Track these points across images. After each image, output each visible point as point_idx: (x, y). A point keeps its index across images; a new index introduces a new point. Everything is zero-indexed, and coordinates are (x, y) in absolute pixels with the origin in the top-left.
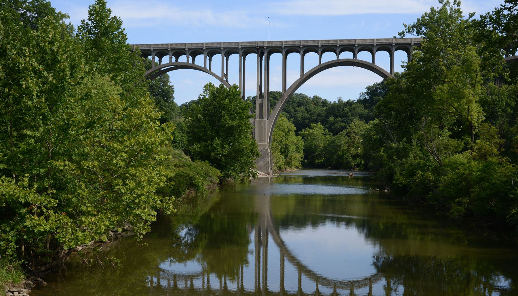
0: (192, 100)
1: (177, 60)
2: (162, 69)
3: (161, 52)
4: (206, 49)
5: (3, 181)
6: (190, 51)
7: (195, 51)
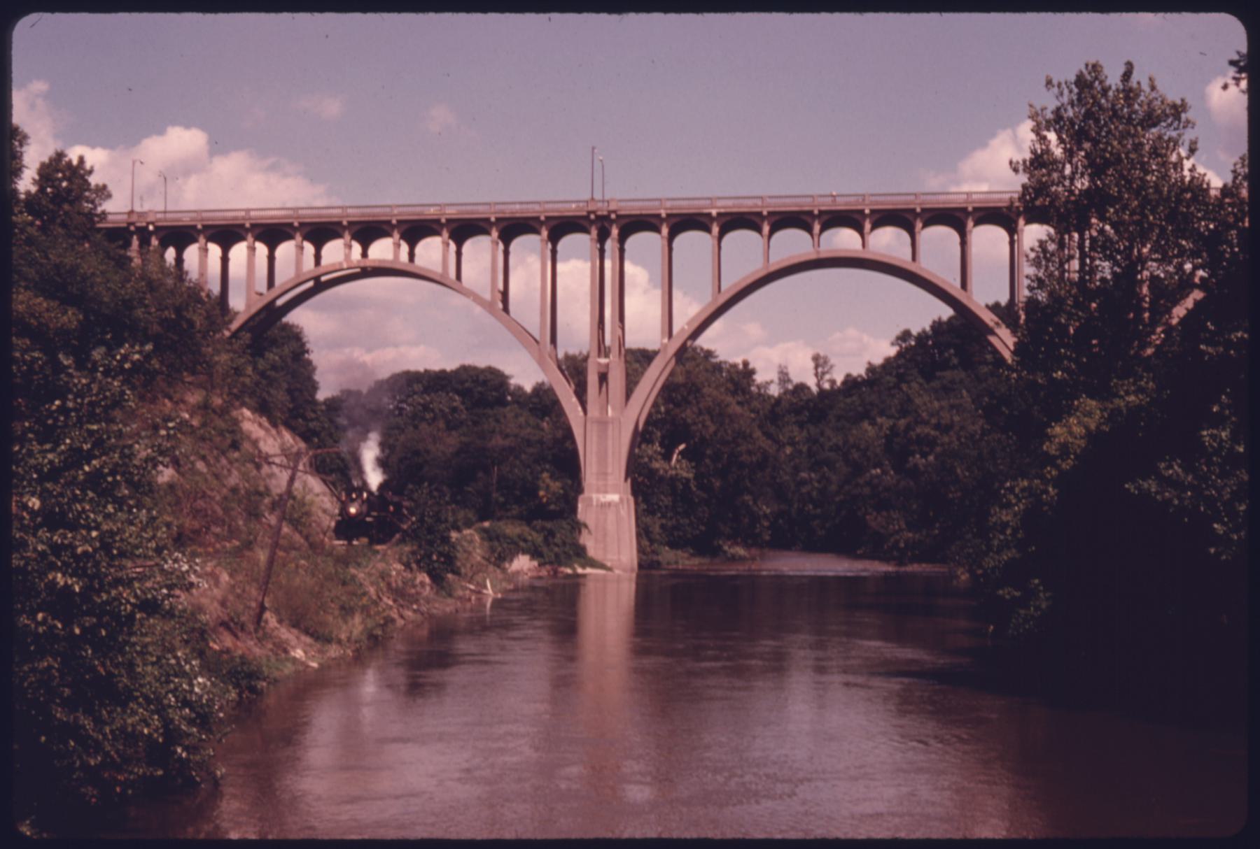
0: (318, 383)
7: (414, 231)
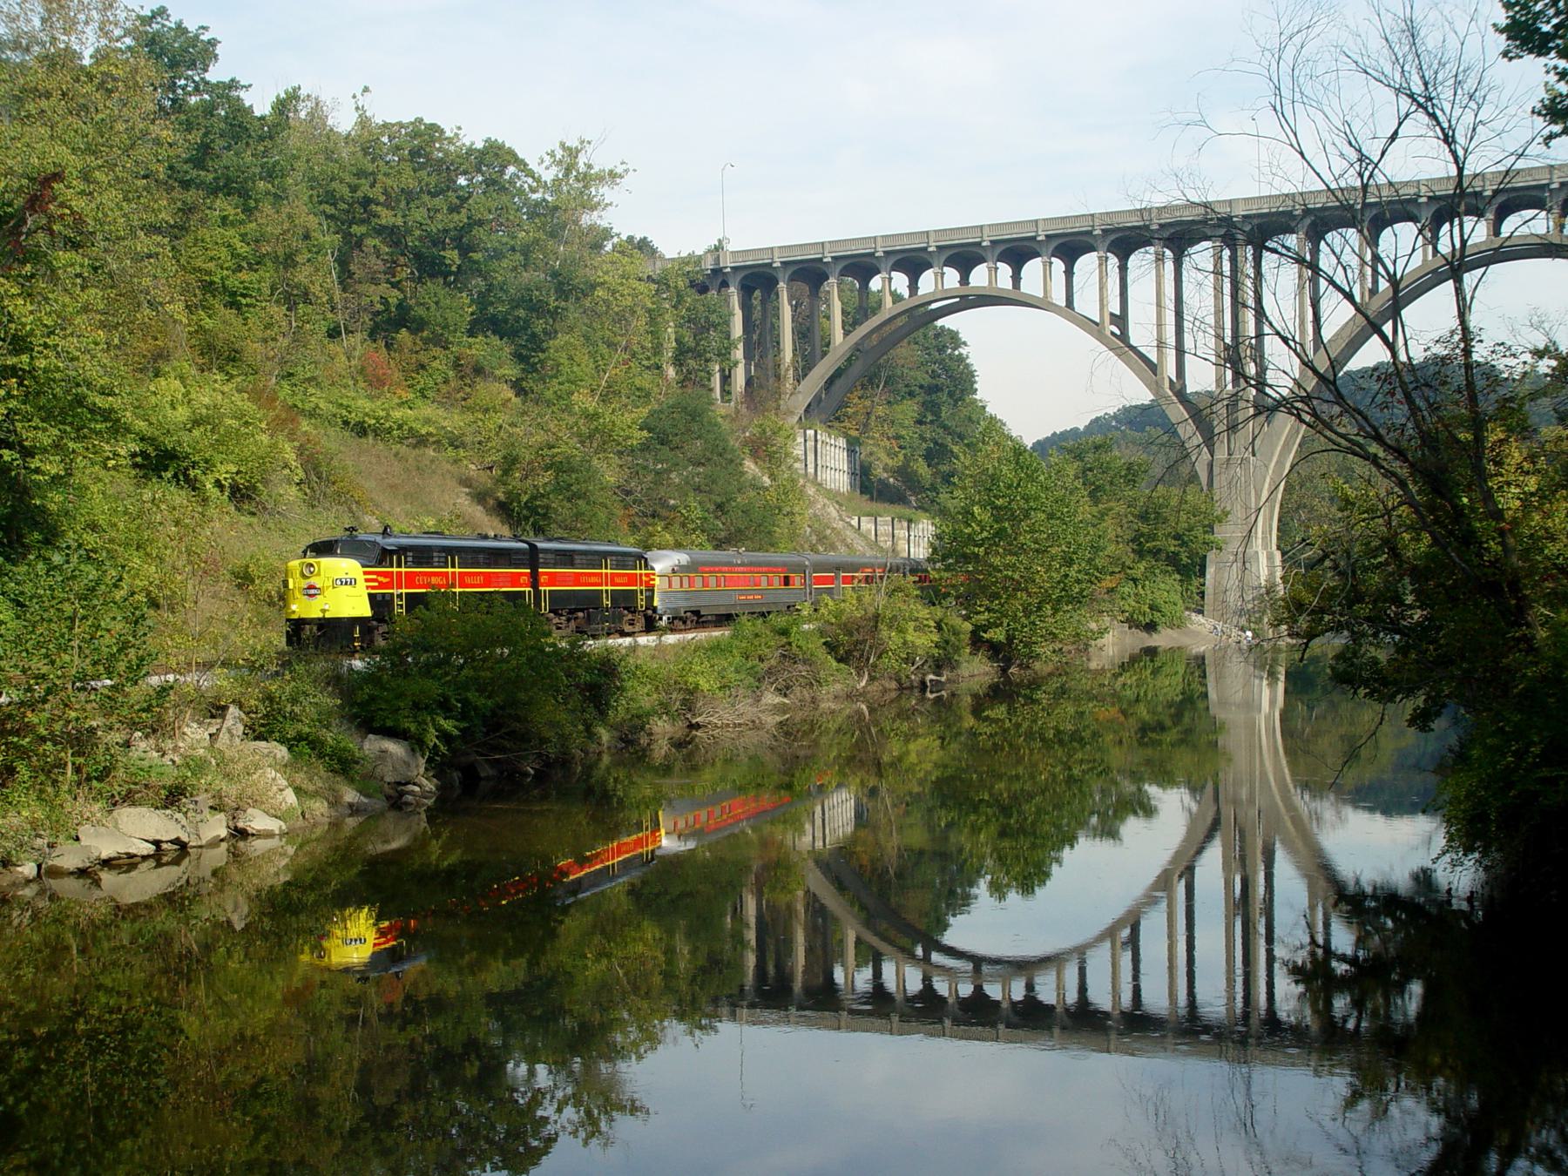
1: (964, 280)
2: (934, 306)
3: (913, 262)
4: (887, 253)
5: (68, 623)
6: (1054, 244)
7: (1017, 252)
